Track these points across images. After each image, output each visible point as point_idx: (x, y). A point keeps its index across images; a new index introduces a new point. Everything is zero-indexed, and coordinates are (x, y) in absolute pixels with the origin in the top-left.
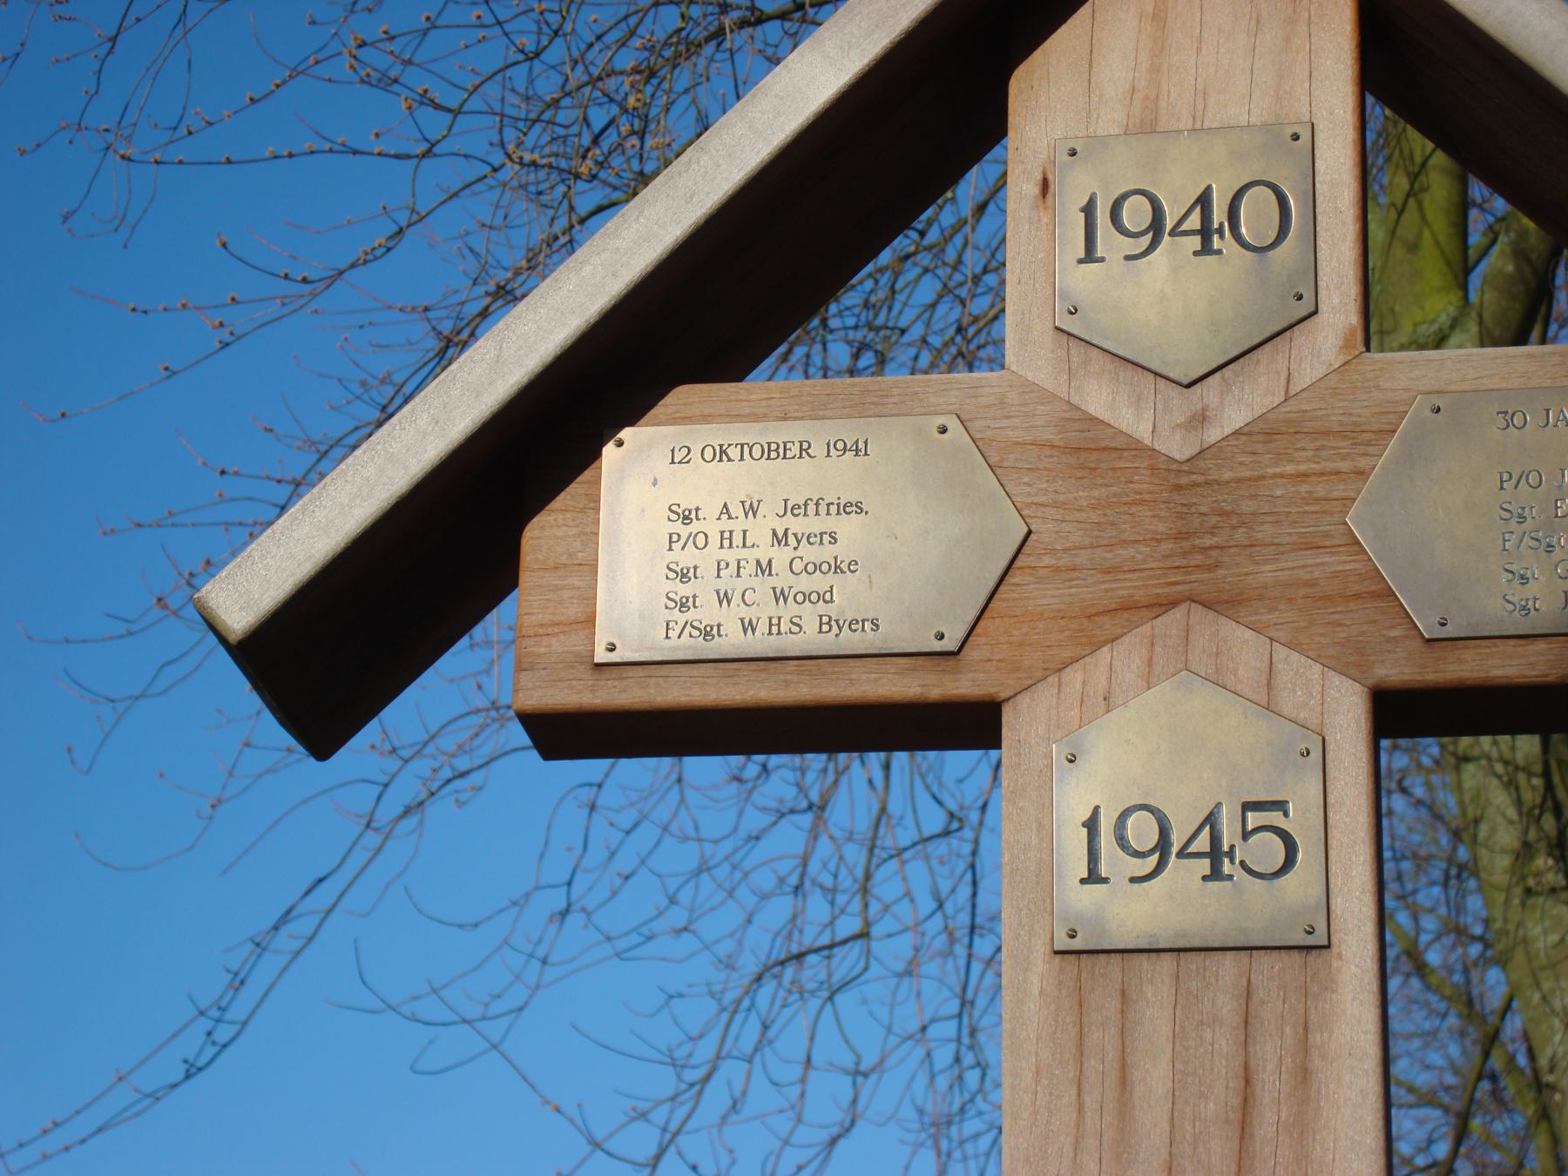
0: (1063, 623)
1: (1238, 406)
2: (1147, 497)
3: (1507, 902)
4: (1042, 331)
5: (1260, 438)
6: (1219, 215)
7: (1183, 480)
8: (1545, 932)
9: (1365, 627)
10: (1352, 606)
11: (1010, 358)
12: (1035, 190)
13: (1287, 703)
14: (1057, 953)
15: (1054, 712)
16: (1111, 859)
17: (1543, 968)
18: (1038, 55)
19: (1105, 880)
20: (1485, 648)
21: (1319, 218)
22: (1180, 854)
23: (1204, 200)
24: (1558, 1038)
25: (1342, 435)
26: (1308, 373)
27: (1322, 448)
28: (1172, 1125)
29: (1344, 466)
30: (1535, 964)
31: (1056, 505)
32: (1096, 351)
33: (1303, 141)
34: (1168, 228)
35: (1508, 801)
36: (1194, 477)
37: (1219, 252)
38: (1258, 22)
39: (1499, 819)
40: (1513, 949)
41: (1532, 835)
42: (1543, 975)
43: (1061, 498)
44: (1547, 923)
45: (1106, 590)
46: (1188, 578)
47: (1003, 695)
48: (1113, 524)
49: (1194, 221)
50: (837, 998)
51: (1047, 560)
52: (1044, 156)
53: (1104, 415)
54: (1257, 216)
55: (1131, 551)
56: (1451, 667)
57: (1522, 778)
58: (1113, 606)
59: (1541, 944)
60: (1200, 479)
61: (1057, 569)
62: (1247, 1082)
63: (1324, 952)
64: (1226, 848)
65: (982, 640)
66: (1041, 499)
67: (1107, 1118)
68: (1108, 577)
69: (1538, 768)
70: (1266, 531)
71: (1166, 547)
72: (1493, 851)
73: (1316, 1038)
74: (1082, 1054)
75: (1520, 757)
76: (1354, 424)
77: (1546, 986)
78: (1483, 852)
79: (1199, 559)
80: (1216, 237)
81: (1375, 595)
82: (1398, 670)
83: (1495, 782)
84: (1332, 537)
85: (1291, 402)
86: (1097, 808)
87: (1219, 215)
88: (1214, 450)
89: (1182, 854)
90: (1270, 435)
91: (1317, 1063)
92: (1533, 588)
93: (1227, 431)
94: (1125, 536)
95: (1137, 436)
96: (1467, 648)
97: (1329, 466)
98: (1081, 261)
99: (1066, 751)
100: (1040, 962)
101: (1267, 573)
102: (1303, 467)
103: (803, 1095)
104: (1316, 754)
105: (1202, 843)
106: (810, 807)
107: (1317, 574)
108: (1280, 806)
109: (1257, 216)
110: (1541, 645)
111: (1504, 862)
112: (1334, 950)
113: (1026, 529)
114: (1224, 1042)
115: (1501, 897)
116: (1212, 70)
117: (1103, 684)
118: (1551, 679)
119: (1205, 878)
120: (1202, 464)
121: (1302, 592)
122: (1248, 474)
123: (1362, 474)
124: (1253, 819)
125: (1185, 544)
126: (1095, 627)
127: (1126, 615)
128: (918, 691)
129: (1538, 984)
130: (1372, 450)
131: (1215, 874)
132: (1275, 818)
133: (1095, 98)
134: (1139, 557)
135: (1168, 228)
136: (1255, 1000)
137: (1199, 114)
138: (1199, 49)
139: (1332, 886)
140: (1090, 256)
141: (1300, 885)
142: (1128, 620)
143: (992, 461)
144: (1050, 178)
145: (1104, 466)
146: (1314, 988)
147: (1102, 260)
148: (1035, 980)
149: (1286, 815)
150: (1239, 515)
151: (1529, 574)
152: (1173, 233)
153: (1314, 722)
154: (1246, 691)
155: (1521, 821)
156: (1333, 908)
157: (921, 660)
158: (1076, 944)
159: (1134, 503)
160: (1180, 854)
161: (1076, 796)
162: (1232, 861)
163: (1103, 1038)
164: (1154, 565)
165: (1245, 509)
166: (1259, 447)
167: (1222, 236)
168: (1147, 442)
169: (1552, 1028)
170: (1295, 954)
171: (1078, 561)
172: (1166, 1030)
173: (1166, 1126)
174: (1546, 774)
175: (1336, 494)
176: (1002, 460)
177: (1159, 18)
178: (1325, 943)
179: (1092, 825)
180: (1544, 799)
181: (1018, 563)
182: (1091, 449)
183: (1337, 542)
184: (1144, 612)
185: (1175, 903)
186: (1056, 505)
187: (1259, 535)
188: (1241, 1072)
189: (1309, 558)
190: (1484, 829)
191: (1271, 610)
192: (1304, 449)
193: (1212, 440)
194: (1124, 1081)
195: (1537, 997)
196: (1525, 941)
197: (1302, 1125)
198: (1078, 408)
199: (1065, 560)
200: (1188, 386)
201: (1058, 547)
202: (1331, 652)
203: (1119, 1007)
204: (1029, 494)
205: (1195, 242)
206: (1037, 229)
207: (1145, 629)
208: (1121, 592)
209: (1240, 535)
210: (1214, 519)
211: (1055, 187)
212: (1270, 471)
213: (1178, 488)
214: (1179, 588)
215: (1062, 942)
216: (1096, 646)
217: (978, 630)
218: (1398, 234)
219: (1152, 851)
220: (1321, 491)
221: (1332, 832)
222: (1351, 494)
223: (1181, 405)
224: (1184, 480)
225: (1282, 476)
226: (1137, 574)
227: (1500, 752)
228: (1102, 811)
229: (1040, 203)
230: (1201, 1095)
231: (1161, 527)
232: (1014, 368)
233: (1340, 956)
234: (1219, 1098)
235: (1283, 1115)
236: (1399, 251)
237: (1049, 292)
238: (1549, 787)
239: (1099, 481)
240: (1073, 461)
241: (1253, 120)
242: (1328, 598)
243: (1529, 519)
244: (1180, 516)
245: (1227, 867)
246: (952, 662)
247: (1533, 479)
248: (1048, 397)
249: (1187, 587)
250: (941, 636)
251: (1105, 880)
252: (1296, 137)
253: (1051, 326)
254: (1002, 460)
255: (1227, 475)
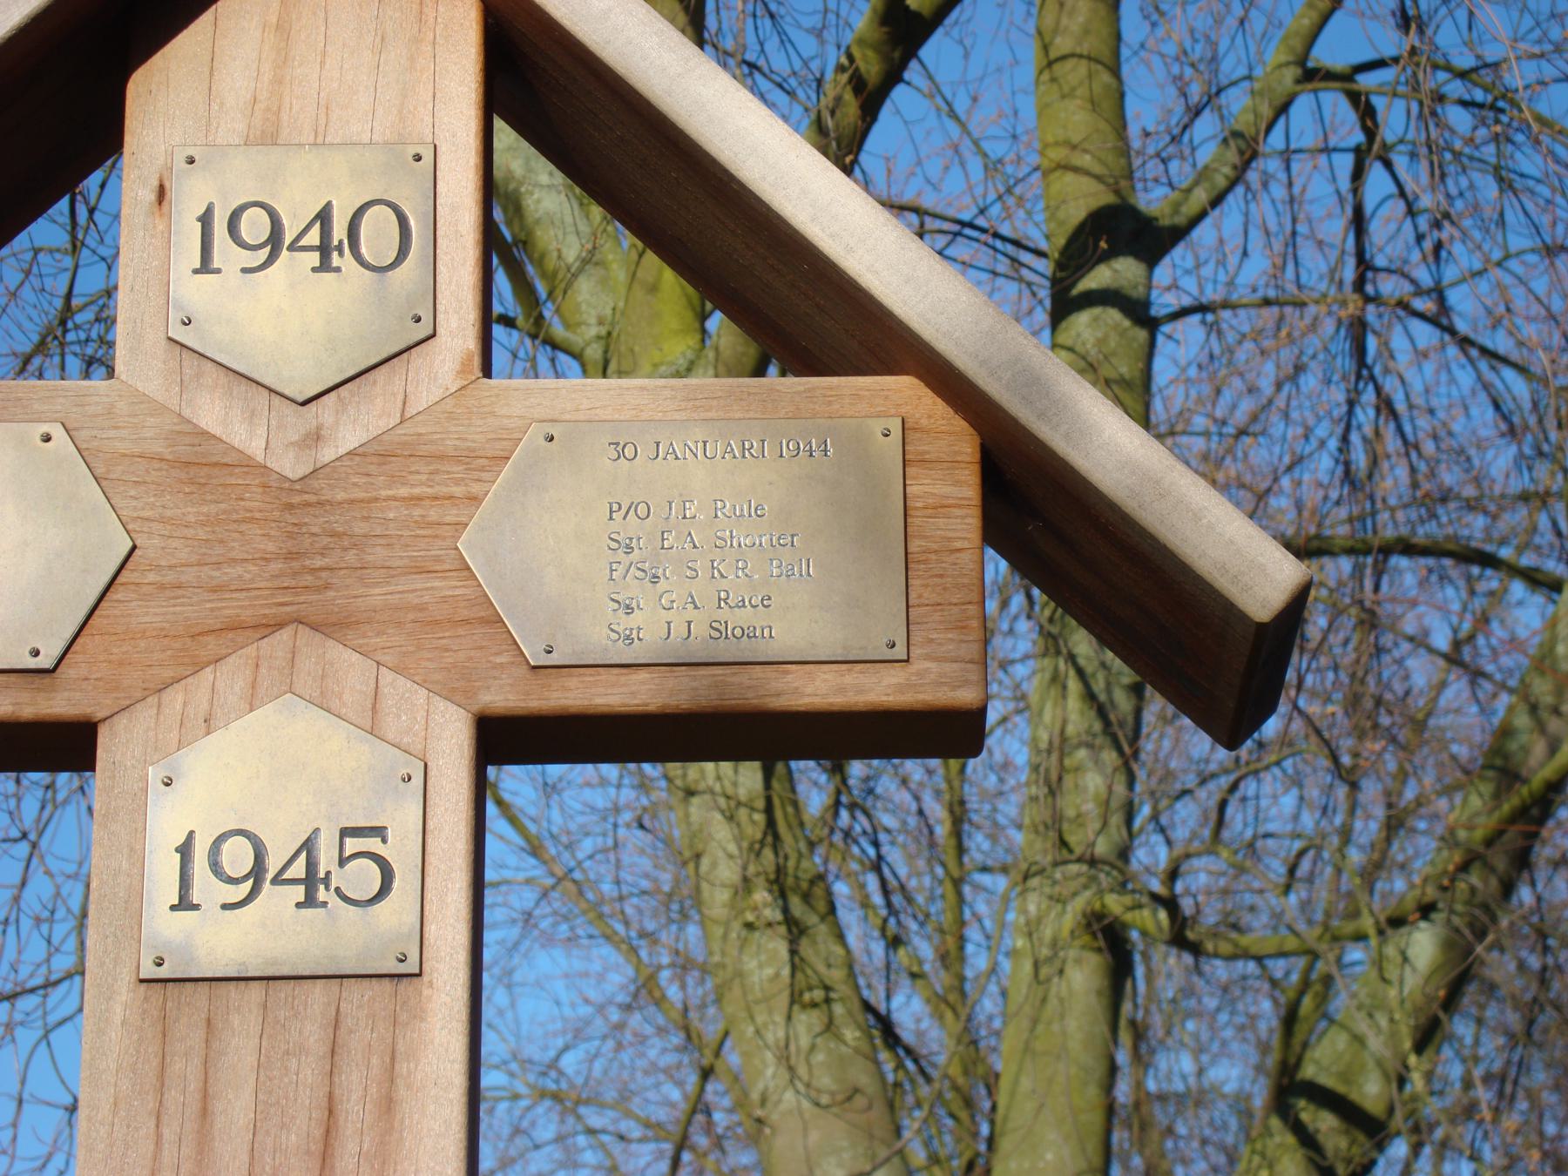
0: (166, 641)
1: (352, 427)
2: (258, 515)
3: (725, 937)
4: (153, 339)
5: (375, 459)
6: (339, 232)
7: (295, 499)
8: (761, 966)
9: (473, 653)
10: (461, 631)
11: (119, 367)
12: (153, 197)
13: (391, 728)
14: (142, 981)
15: (151, 734)
16: (204, 885)
17: (757, 1002)
18: (157, 60)
19: (196, 907)
20: (589, 676)
21: (439, 241)
22: (275, 881)
23: (324, 217)
24: (770, 1071)
25: (457, 459)
26: (423, 398)
27: (436, 472)
28: (252, 1157)
29: (458, 491)
30: (750, 998)
31: (162, 520)
32: (210, 364)
33: (427, 162)
34: (287, 242)
35: (730, 837)
36: (306, 497)
37: (338, 270)
38: (383, 39)
39: (721, 854)
40: (732, 980)
41: (752, 869)
42: (757, 1009)
43: (168, 513)
44: (763, 958)
45: (212, 610)
46: (297, 599)
47: (100, 715)
48: (221, 541)
49: (313, 237)
50: (52, 1036)
51: (151, 577)
52: (161, 161)
53: (217, 430)
54: (378, 234)
55: (239, 570)
56: (555, 695)
57: (743, 813)
58: (218, 626)
59: (756, 979)
60: (312, 498)
61: (162, 587)
62: (331, 1112)
63: (415, 979)
64: (322, 875)
65: (79, 658)
66: (148, 513)
67: (185, 1151)
68: (215, 596)
69: (760, 804)
70: (378, 554)
71: (276, 566)
72: (713, 885)
73: (402, 1068)
74: (163, 1085)
75: (742, 793)
76: (468, 449)
77: (760, 1019)
78: (704, 885)
79: (308, 579)
80: (335, 254)
81: (484, 621)
82: (505, 697)
83: (719, 816)
84: (443, 561)
85: (406, 425)
86: (191, 833)
87: (339, 232)
88: (328, 469)
89: (276, 881)
90: (385, 456)
91: (402, 1092)
92: (637, 619)
93: (342, 451)
94: (233, 554)
95: (249, 452)
96: (571, 675)
97: (443, 490)
98: (196, 272)
99: (163, 774)
100: (124, 990)
101: (377, 596)
102: (417, 491)
103: (14, 1139)
104: (418, 780)
105: (298, 869)
106: (24, 835)
107: (426, 599)
108: (379, 832)
109: (378, 234)
110: (643, 675)
111: (723, 896)
112: (425, 978)
113: (130, 544)
114: (310, 1072)
115: (718, 931)
116: (335, 85)
117: (205, 706)
118: (651, 708)
119: (298, 905)
120: (315, 484)
121: (411, 616)
122: (362, 495)
123: (475, 500)
124: (352, 845)
125: (295, 564)
126: (197, 648)
127: (230, 635)
128: (10, 709)
129: (752, 1018)
130: (485, 476)
131: (310, 901)
132: (373, 844)
133: (215, 107)
134: (248, 576)
135: (287, 242)
136: (342, 1031)
137: (321, 130)
138: (322, 63)
139: (426, 913)
140: (206, 266)
141: (397, 912)
142: (232, 640)
143: (98, 472)
144: (167, 185)
145: (214, 481)
146: (403, 1017)
147: (218, 271)
148: (118, 1009)
149: (384, 841)
150: (351, 536)
151: (634, 605)
152: (291, 248)
153: (417, 747)
154: (351, 716)
155: (741, 857)
156: (426, 935)
157: (13, 677)
158: (163, 972)
159: (244, 521)
160: (275, 881)
161: (168, 821)
162: (327, 889)
163: (186, 1068)
164: (262, 585)
165: (357, 531)
166: (373, 469)
167: (341, 254)
168: (260, 458)
169: (764, 1062)
170: (386, 981)
171: (184, 578)
172: (251, 1060)
173: (245, 1158)
174: (769, 810)
175: (448, 519)
176: (108, 472)
177: (283, 29)
178: (417, 971)
179: (185, 850)
180: (765, 834)
181: (121, 579)
182: (200, 464)
183: (447, 567)
184: (249, 633)
185: (270, 931)
186: (162, 520)
187: (370, 558)
188: (325, 1104)
189: (419, 582)
190: (705, 863)
191: (378, 634)
192: (418, 473)
193: (326, 460)
194: (205, 1112)
195: (751, 1030)
196: (740, 974)
197: (384, 1152)
198: (189, 422)
199: (170, 577)
200: (304, 404)
201: (163, 563)
202: (437, 677)
203: (204, 1036)
204: (135, 508)
205: (314, 258)
206: (152, 236)
207: (251, 650)
208: (227, 612)
209: (351, 557)
210: (326, 540)
211: (172, 194)
212: (384, 493)
213: (290, 507)
214: (288, 609)
215: (148, 970)
216: (199, 667)
217: (75, 648)
218: (639, 274)
219: (246, 878)
220: (433, 515)
221: (430, 859)
222: (464, 519)
223: (298, 422)
224: (296, 499)
225: (395, 499)
226: (244, 594)
227: (722, 787)
228: (197, 836)
229: (156, 209)
230: (283, 1126)
231: (271, 547)
232: (123, 377)
233: (431, 982)
234: (301, 1129)
235: (365, 1146)
236: (638, 293)
237: (162, 301)
238: (771, 823)
239: (209, 497)
240: (183, 476)
241: (376, 138)
242: (437, 622)
243: (636, 551)
244: (290, 535)
245: (322, 894)
246: (47, 680)
247: (642, 510)
248: (160, 409)
249: (294, 608)
250: (36, 653)
251: (196, 907)
252: (418, 158)
253: (163, 336)
254: (108, 472)
255: (341, 496)
